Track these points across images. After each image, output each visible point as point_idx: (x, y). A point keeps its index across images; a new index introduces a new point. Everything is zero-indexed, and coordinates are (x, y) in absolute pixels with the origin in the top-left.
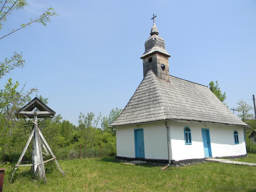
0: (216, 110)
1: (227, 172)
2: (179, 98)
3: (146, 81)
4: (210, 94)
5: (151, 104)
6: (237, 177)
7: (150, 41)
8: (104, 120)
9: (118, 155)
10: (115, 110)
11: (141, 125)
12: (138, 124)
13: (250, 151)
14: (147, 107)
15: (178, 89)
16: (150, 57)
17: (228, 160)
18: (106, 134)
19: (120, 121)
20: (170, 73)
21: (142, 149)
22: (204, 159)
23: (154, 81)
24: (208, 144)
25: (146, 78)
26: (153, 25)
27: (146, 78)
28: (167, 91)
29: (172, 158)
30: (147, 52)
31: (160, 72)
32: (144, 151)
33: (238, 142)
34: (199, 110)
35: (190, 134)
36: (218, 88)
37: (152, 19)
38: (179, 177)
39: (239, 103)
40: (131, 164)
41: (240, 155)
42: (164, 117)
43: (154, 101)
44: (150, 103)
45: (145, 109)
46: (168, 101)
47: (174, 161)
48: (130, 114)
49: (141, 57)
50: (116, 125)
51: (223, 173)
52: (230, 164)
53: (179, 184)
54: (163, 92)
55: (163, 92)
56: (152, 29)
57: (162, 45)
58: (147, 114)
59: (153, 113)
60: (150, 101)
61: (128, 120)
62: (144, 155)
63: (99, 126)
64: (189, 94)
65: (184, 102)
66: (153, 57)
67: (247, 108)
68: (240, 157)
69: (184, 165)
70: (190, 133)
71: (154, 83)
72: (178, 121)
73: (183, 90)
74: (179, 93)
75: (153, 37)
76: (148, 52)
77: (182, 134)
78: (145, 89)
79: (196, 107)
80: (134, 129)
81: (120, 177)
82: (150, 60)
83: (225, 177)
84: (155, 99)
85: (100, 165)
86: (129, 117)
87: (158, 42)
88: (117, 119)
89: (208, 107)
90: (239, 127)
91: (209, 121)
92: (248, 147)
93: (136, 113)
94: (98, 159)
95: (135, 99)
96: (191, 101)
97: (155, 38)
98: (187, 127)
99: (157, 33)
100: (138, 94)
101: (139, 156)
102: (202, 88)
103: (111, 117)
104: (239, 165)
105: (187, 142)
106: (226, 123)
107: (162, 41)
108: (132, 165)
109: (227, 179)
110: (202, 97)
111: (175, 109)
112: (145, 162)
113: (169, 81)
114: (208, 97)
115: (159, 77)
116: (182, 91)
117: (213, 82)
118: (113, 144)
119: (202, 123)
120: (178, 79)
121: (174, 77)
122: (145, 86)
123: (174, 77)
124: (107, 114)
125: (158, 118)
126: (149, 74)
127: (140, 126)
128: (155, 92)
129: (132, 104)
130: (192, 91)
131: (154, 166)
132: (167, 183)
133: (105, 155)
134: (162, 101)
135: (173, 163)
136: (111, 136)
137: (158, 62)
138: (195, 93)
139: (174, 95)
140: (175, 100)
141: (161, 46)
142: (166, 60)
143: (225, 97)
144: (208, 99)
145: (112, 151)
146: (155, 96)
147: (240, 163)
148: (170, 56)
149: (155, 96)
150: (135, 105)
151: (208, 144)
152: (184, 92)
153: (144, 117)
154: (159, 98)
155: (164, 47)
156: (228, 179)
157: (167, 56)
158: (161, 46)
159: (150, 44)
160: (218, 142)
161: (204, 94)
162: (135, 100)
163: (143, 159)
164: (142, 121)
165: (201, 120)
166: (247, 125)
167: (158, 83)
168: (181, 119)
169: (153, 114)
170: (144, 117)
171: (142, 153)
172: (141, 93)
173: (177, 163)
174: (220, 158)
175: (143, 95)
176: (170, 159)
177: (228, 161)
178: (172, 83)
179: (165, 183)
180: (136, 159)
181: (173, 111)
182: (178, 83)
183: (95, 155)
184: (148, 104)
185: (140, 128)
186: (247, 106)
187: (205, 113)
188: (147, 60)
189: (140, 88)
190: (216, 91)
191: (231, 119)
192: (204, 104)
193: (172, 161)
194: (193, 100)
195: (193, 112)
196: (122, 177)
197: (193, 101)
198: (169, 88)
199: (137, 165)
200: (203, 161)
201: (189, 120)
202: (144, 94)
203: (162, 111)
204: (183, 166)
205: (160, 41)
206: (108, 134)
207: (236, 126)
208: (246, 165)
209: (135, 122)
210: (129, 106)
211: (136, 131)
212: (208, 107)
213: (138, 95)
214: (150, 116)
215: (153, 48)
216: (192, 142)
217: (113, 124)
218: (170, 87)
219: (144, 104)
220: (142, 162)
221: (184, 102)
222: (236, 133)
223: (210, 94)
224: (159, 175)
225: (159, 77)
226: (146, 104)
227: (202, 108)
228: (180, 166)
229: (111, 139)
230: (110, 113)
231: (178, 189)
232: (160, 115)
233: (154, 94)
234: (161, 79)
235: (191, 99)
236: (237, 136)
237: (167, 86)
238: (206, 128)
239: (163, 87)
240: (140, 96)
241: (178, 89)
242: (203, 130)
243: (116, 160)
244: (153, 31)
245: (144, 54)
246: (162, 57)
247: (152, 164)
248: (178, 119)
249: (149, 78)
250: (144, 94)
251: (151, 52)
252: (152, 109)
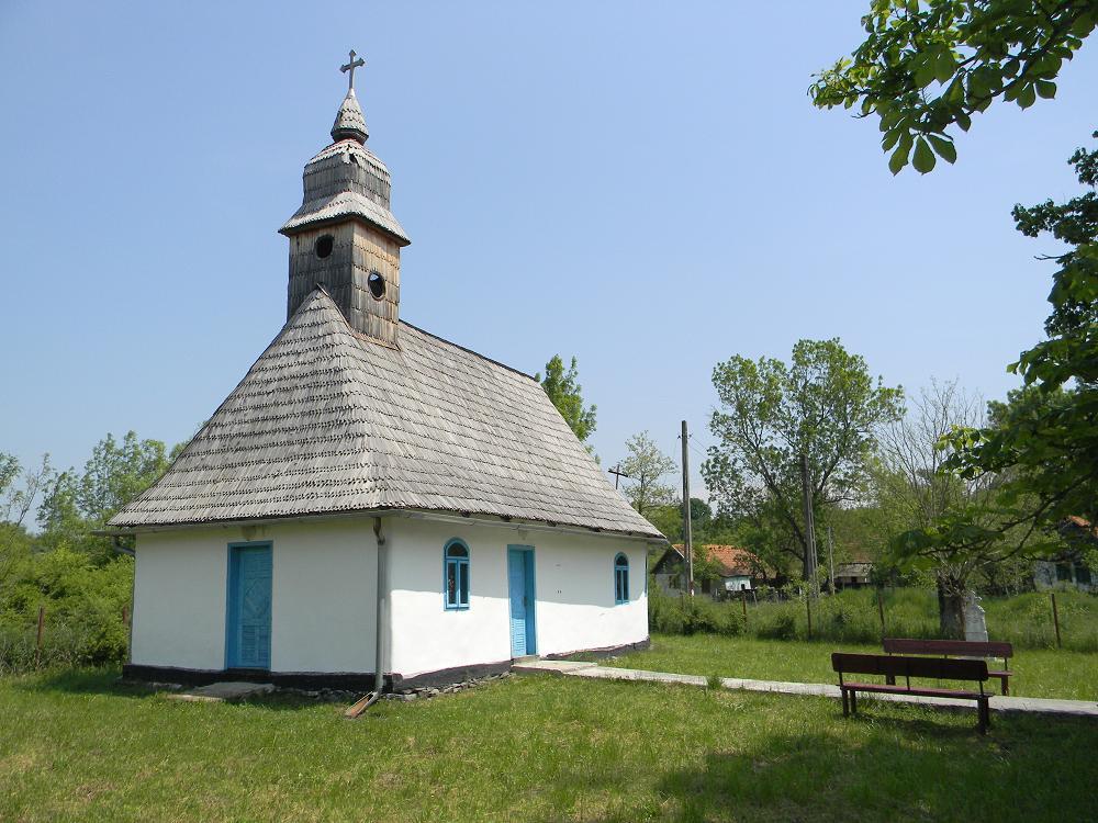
0: (561, 474)
1: (594, 711)
2: (432, 421)
3: (299, 333)
4: (545, 409)
5: (315, 440)
6: (625, 729)
7: (328, 163)
8: (57, 488)
9: (140, 657)
10: (119, 445)
11: (263, 527)
12: (248, 524)
13: (659, 625)
14: (296, 448)
15: (431, 382)
16: (322, 233)
17: (590, 664)
18: (62, 554)
19: (164, 504)
20: (403, 312)
21: (257, 631)
22: (509, 666)
23: (337, 341)
24: (525, 607)
25: (298, 323)
26: (348, 97)
27: (298, 323)
28: (389, 386)
29: (390, 665)
30: (313, 211)
31: (364, 303)
32: (266, 637)
33: (626, 597)
34: (503, 472)
35: (465, 568)
36: (575, 387)
37: (344, 69)
38: (418, 746)
39: (634, 442)
40: (208, 699)
41: (629, 643)
42: (373, 500)
43: (328, 425)
44: (311, 434)
45: (287, 459)
46: (389, 433)
47: (398, 676)
48: (212, 475)
49: (281, 226)
50: (142, 520)
51: (579, 717)
52: (599, 678)
53: (421, 773)
54: (373, 392)
55: (373, 392)
56: (341, 114)
57: (378, 189)
58: (296, 479)
59: (323, 476)
60: (314, 426)
61: (199, 501)
62: (266, 655)
64: (472, 406)
65: (452, 438)
66: (339, 235)
67: (657, 466)
68: (630, 653)
69: (436, 691)
71: (336, 350)
72: (428, 516)
73: (447, 388)
74: (434, 401)
75: (344, 150)
76: (318, 211)
77: (436, 565)
78: (295, 370)
79: (495, 459)
80: (511, 542)
81: (164, 763)
82: (324, 247)
83: (586, 732)
84: (334, 416)
85: (46, 708)
86: (208, 488)
87: (362, 177)
88: (144, 496)
89: (537, 460)
90: (636, 540)
91: (537, 519)
92: (653, 613)
93: (243, 472)
94: (33, 678)
95: (240, 410)
96: (475, 435)
98: (457, 539)
99: (359, 137)
100: (255, 389)
101: (241, 663)
102: (518, 385)
103: (94, 477)
104: (627, 682)
105: (452, 600)
106: (595, 525)
107: (380, 175)
108: (209, 704)
109: (593, 740)
110: (516, 420)
111: (418, 465)
112: (269, 687)
113: (394, 347)
114: (536, 420)
116: (442, 390)
117: (560, 362)
118: (103, 604)
119: (513, 526)
120: (431, 338)
121: (416, 329)
122: (292, 359)
123: (416, 329)
124: (74, 457)
125: (343, 503)
126: (314, 305)
127: (259, 532)
128: (337, 389)
129: (227, 430)
130: (482, 393)
131: (312, 702)
132: (377, 771)
133: (62, 659)
134: (366, 428)
135: (394, 685)
136: (88, 566)
137: (357, 261)
138: (493, 404)
139: (413, 405)
140: (419, 429)
141: (374, 192)
142: (390, 258)
143: (594, 422)
144: (537, 428)
145: (99, 640)
146: (335, 403)
147: (632, 674)
148: (408, 243)
149: (335, 403)
150: (239, 435)
151: (525, 607)
152: (452, 398)
153: (281, 493)
154: (354, 415)
155: (385, 200)
156: (597, 738)
157: (394, 241)
158: (374, 192)
159: (325, 178)
160: (560, 597)
161: (524, 407)
162: (240, 416)
163: (263, 676)
164: (270, 509)
165: (511, 512)
166: (659, 533)
167: (354, 351)
168: (440, 510)
169: (325, 483)
170: (281, 493)
171: (256, 646)
172: (274, 386)
173: (410, 685)
174: (565, 657)
175: (283, 397)
176: (384, 671)
177: (593, 670)
178: (409, 357)
179: (368, 774)
180: (229, 675)
181: (409, 475)
182: (429, 355)
183: (9, 662)
184: (303, 435)
185: (258, 538)
186: (655, 457)
187: (526, 486)
188: (309, 243)
189: (269, 364)
190: (566, 396)
191: (610, 509)
192: (521, 447)
193: (388, 678)
194: (484, 431)
195: (483, 480)
196: (170, 763)
197: (483, 436)
198: (394, 377)
199: (235, 700)
200: (506, 673)
201: (467, 514)
202: (286, 390)
203: (366, 472)
204: (430, 696)
205: (373, 170)
206: (70, 556)
207: (620, 538)
208: (653, 683)
209: (236, 512)
210: (209, 438)
211: (236, 552)
212: (537, 460)
213: (259, 394)
214: (309, 490)
215: (341, 196)
216: (471, 598)
217: (121, 518)
218: (399, 370)
219: (284, 437)
220: (257, 687)
221: (452, 438)
222: (622, 561)
223: (545, 409)
224: (338, 741)
226: (295, 436)
227: (515, 463)
228: (418, 696)
229: (87, 580)
230: (92, 457)
231: (420, 793)
232: (354, 487)
233: (334, 397)
234: (364, 332)
235: (476, 425)
236: (626, 573)
237: (388, 365)
238: (525, 543)
239: (372, 371)
240: (266, 400)
241: (431, 382)
242: (513, 551)
243: (127, 682)
244: (345, 124)
245: (296, 216)
247: (304, 693)
248: (426, 509)
249: (313, 325)
250: (286, 390)
251: (328, 212)
252: (319, 462)
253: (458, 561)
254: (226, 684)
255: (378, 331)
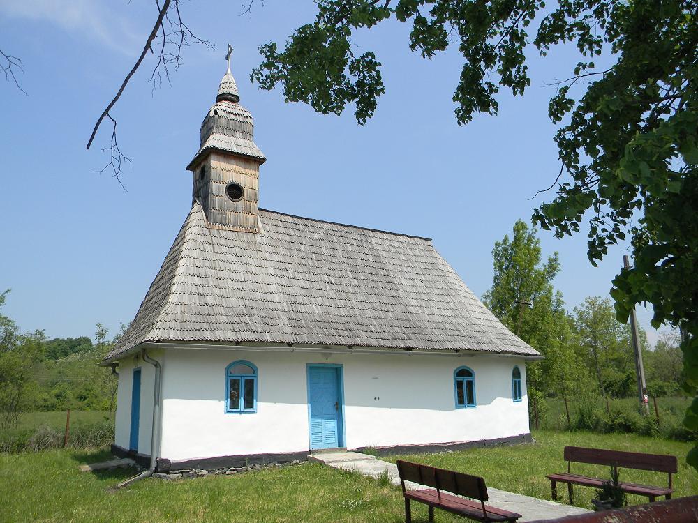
47: (166, 461)
63: (678, 329)
70: (253, 380)
80: (310, 362)
87: (223, 122)
97: (216, 113)
107: (240, 119)
115: (214, 220)
155: (247, 134)
158: (235, 131)
166: (539, 354)
205: (233, 117)
207: (449, 355)
225: (214, 220)
242: (314, 370)
246: (233, 161)
253: (465, 379)
254: (651, 452)
255: (240, 223)
